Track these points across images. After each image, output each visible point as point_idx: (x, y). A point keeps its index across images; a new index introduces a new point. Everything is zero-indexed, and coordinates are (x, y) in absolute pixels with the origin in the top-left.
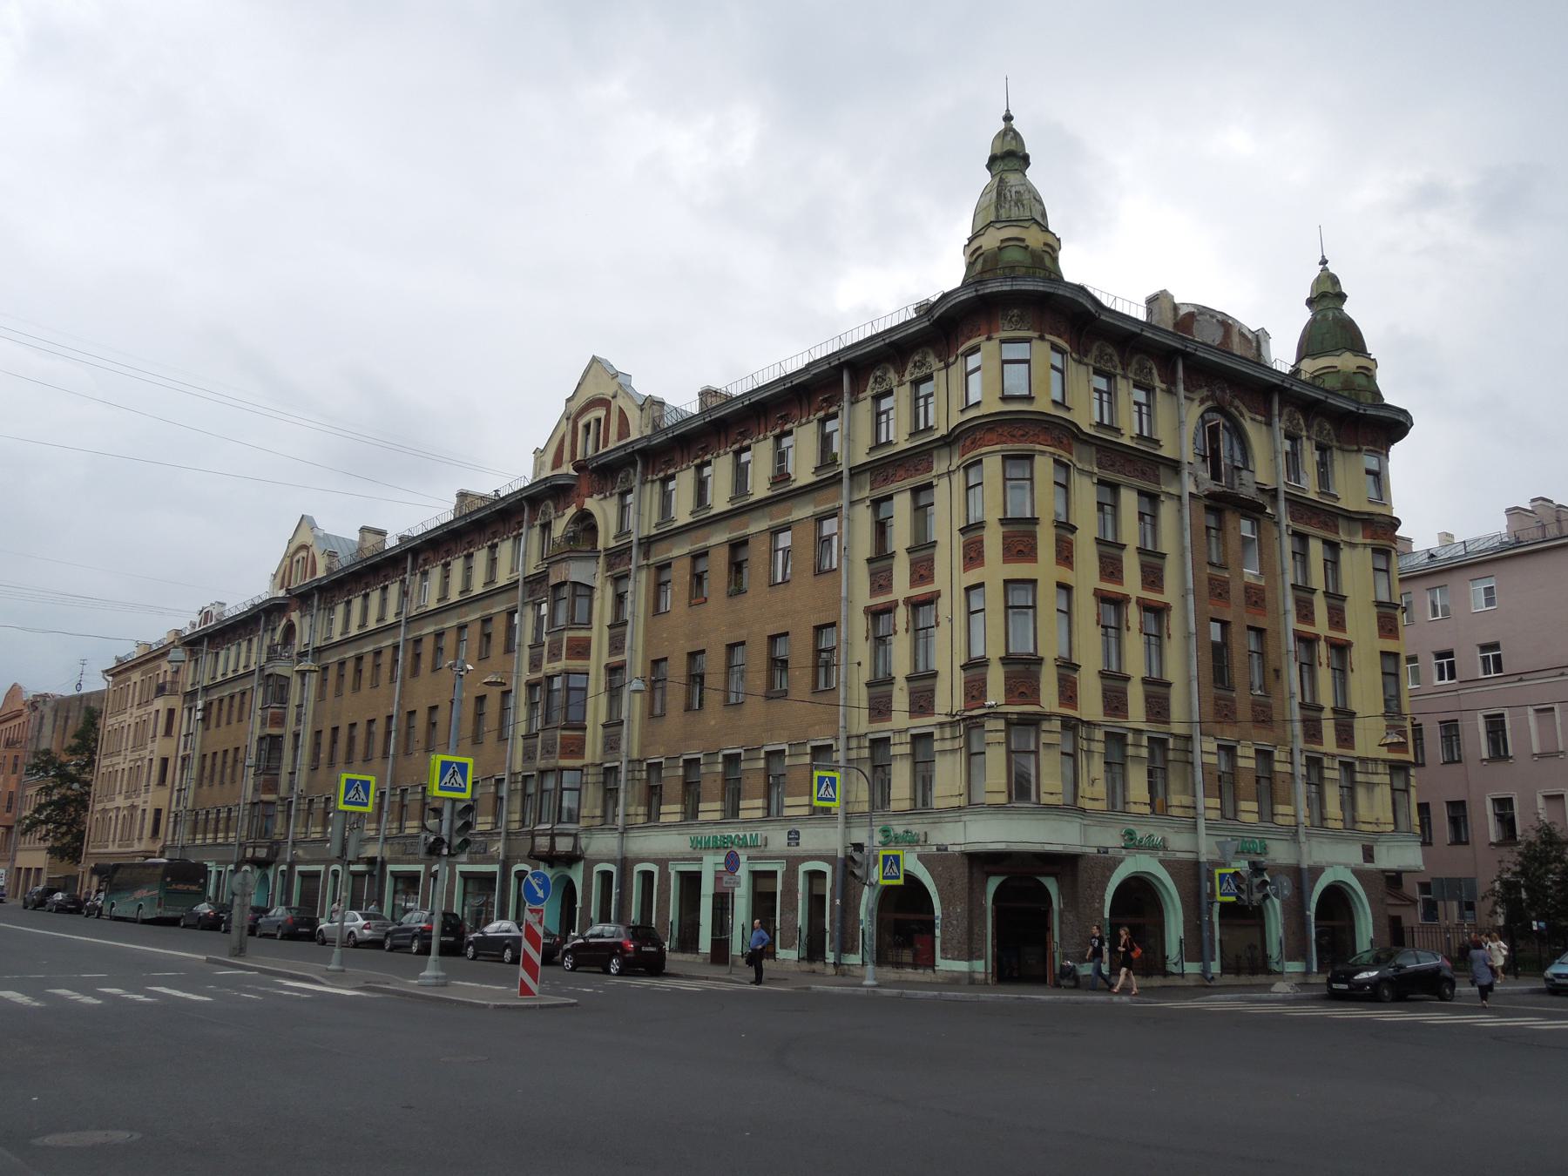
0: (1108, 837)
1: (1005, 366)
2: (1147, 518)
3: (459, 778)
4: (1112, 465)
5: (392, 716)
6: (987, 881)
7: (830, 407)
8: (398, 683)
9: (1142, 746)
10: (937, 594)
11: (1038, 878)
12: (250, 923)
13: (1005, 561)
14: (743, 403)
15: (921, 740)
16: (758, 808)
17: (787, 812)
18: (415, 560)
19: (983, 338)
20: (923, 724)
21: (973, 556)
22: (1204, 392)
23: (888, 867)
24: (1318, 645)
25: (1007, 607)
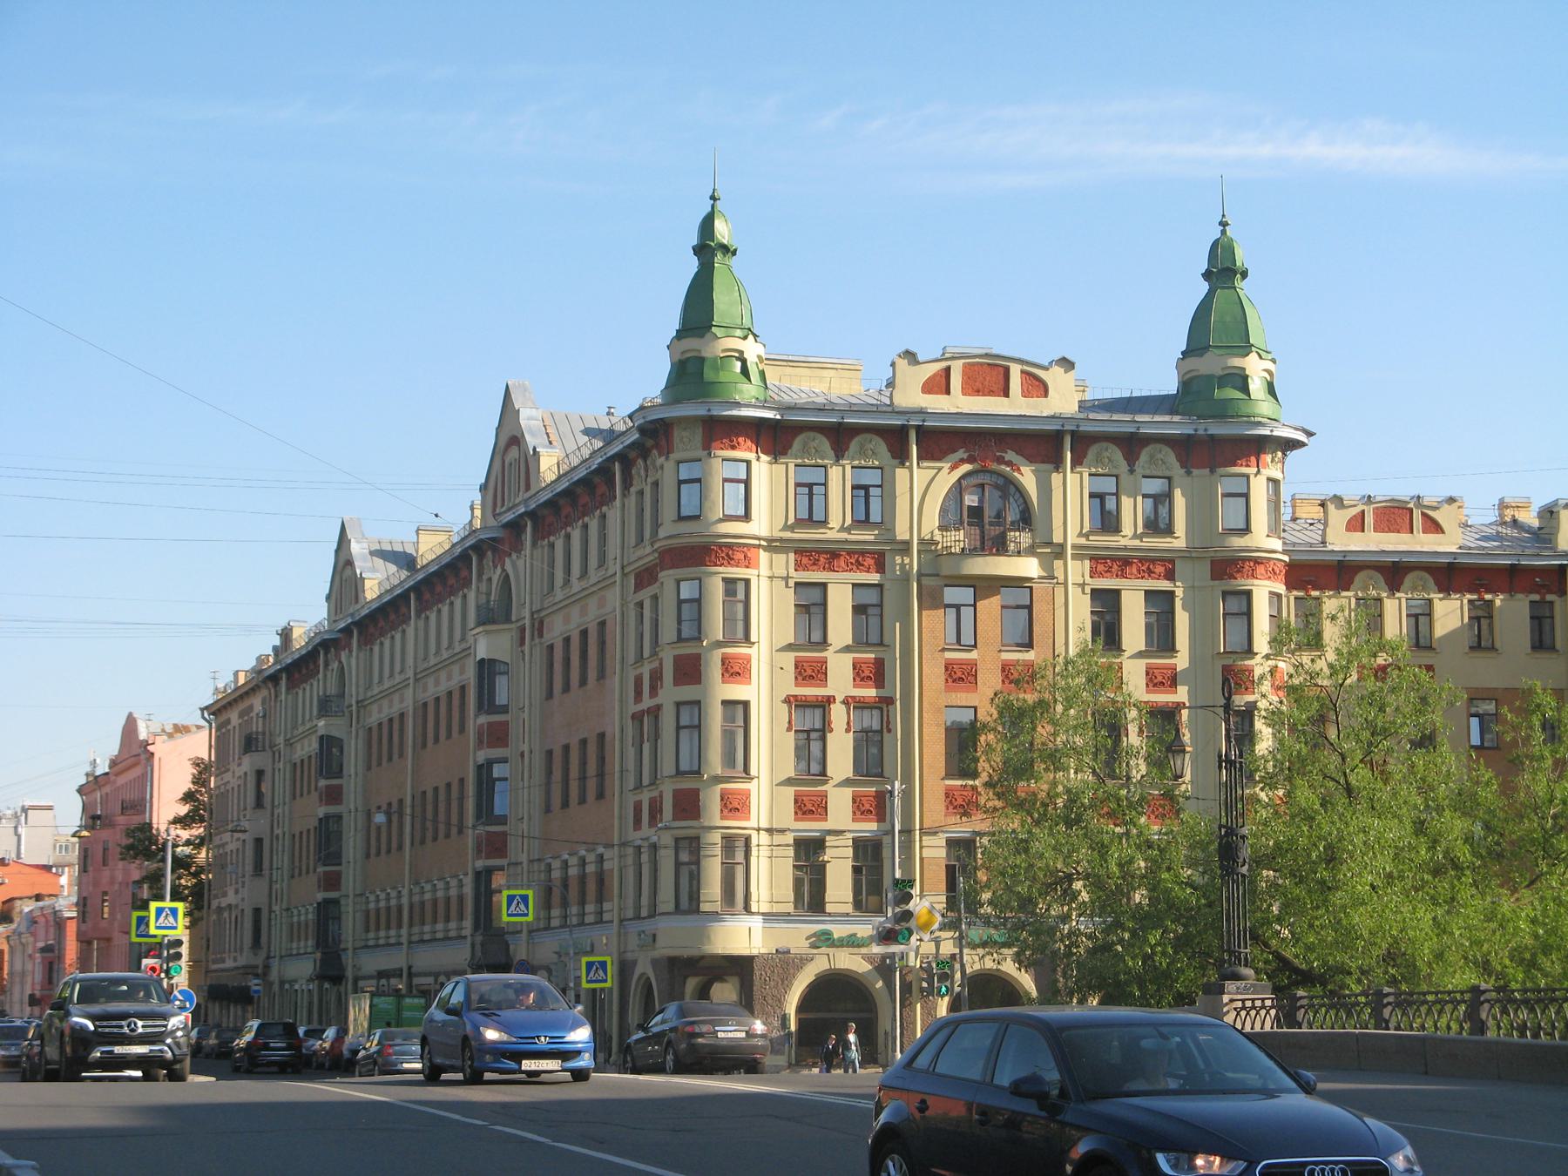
0: (796, 936)
3: (522, 906)
4: (814, 564)
6: (685, 983)
18: (419, 599)
22: (961, 454)
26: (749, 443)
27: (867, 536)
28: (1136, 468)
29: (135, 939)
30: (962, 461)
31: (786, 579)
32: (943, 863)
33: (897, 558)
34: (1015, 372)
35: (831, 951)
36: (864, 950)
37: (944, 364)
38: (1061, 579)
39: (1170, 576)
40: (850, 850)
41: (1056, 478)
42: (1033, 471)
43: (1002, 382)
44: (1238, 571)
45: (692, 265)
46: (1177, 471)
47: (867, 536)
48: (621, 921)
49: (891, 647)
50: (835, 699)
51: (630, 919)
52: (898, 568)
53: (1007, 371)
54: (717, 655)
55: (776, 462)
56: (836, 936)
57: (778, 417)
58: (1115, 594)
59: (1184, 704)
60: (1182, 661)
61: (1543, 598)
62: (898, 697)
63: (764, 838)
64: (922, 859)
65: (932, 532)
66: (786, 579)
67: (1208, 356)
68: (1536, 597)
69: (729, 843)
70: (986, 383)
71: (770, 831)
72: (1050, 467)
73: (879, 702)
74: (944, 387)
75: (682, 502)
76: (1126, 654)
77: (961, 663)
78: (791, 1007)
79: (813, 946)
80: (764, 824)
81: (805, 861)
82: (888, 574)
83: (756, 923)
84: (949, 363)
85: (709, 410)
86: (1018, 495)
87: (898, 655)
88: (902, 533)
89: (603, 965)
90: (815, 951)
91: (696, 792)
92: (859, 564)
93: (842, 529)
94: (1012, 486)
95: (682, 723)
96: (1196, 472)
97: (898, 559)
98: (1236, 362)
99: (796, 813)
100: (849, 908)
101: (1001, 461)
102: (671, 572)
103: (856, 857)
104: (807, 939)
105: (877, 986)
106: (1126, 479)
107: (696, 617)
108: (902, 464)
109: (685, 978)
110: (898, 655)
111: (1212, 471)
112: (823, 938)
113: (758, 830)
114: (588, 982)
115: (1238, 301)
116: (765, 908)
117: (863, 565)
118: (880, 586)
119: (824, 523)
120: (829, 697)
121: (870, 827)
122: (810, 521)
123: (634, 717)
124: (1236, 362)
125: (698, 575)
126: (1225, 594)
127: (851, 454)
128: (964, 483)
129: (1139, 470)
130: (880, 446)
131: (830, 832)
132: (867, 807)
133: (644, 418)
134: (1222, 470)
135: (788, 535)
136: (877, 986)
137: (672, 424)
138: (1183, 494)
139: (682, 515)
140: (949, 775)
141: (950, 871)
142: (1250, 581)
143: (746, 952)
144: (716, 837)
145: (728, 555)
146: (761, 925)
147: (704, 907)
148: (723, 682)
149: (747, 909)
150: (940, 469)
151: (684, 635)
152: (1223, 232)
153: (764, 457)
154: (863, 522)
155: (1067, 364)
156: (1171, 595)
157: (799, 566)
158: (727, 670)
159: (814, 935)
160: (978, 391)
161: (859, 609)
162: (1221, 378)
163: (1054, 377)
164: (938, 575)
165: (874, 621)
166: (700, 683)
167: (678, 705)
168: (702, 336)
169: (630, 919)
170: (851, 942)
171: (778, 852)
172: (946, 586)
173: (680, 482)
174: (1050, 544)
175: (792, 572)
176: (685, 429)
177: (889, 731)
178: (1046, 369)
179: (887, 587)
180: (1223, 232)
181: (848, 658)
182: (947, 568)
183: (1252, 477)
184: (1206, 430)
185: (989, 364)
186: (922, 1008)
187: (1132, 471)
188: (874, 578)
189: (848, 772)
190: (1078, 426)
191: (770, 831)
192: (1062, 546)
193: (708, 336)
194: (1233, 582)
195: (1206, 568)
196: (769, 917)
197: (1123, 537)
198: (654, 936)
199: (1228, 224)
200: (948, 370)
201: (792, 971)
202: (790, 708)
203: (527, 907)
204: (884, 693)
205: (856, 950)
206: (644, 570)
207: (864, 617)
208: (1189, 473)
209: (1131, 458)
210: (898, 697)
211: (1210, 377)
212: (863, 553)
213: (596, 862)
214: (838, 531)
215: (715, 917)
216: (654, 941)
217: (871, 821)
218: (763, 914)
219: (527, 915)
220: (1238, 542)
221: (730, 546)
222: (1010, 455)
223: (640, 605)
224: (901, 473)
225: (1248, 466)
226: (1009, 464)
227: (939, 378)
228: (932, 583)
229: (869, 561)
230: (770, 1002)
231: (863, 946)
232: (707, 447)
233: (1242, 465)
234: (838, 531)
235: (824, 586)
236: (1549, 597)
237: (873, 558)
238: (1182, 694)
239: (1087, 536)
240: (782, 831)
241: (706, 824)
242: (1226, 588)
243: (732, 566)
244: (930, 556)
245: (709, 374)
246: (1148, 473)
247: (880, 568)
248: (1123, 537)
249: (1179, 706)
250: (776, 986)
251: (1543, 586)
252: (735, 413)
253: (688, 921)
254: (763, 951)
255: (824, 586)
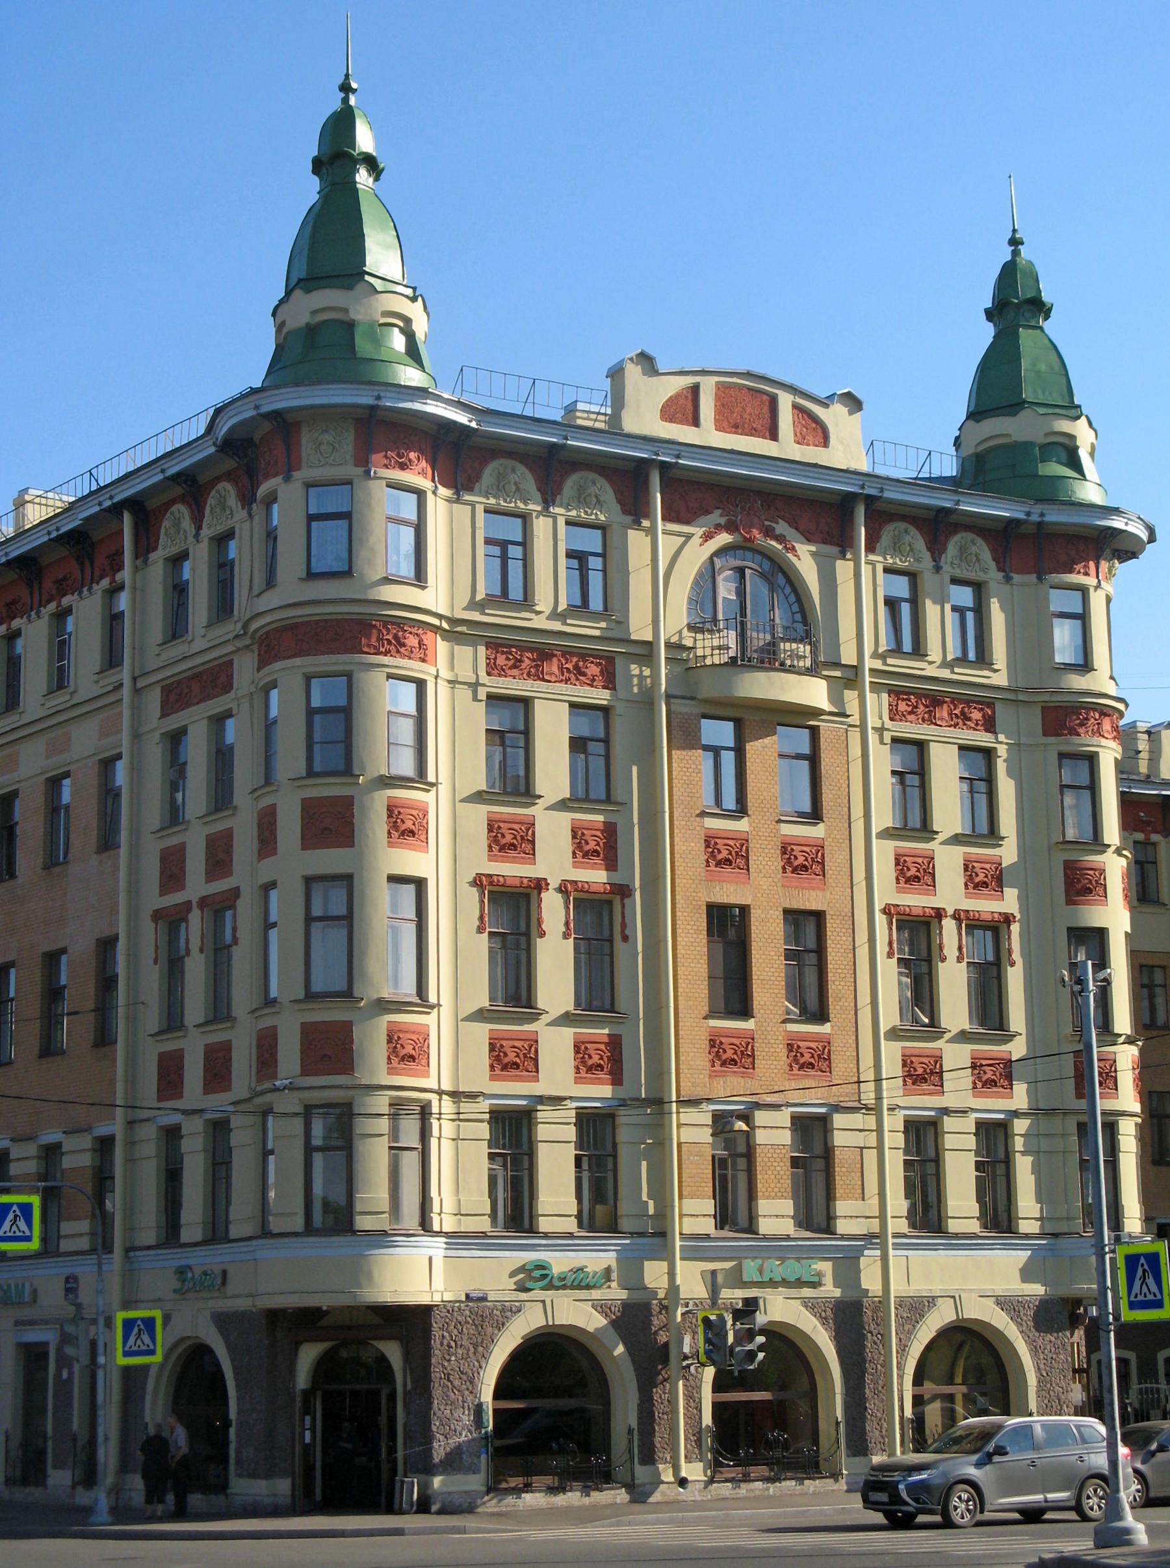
1: (314, 524)
2: (596, 748)
3: (22, 1224)
4: (514, 667)
5: (114, 939)
6: (296, 1354)
7: (13, 618)
8: (123, 851)
9: (1021, 1135)
10: (235, 893)
11: (334, 1343)
12: (1132, 1537)
13: (303, 849)
14: (100, 504)
15: (219, 1128)
16: (81, 1235)
17: (65, 1245)
19: (279, 479)
20: (220, 1101)
21: (267, 842)
22: (716, 517)
23: (1137, 1283)
24: (941, 928)
25: (309, 919)
26: (424, 464)
27: (592, 629)
28: (942, 563)
29: (120, 1316)
30: (719, 528)
31: (475, 686)
32: (709, 1152)
33: (633, 666)
34: (785, 401)
35: (548, 1295)
36: (596, 1294)
37: (689, 380)
38: (855, 719)
39: (990, 725)
40: (572, 1130)
41: (844, 569)
42: (813, 554)
43: (768, 416)
44: (1082, 725)
45: (310, 189)
46: (993, 575)
47: (592, 629)
48: (128, 1250)
49: (626, 805)
50: (548, 884)
51: (149, 1248)
52: (635, 681)
53: (773, 402)
54: (380, 799)
55: (458, 500)
56: (556, 1270)
57: (474, 425)
58: (921, 746)
59: (1014, 917)
60: (1008, 853)
61: (1148, 839)
62: (637, 884)
63: (447, 1105)
64: (679, 1145)
65: (680, 632)
66: (475, 686)
67: (1025, 415)
68: (1140, 836)
69: (398, 1108)
70: (746, 416)
71: (455, 1095)
72: (834, 550)
73: (612, 892)
74: (690, 416)
75: (314, 552)
76: (940, 838)
77: (727, 836)
78: (487, 1395)
79: (522, 1288)
80: (446, 1086)
81: (510, 1148)
82: (621, 693)
83: (436, 1247)
84: (697, 379)
85: (378, 398)
86: (788, 590)
87: (636, 820)
88: (640, 630)
89: (149, 1323)
90: (524, 1296)
91: (346, 1028)
92: (579, 672)
93: (554, 615)
94: (780, 575)
95: (317, 911)
96: (1016, 578)
97: (635, 669)
98: (1065, 426)
99: (492, 1067)
100: (571, 1225)
101: (769, 533)
102: (297, 661)
103: (580, 1144)
104: (512, 1275)
105: (616, 1353)
106: (929, 580)
107: (341, 736)
108: (637, 524)
109: (298, 1344)
110: (636, 820)
111: (1040, 578)
112: (537, 1273)
113: (440, 1093)
114: (126, 1354)
115: (1049, 345)
116: (449, 1225)
117: (584, 674)
118: (605, 710)
119: (527, 602)
120: (539, 880)
121: (600, 1092)
122: (501, 599)
123: (157, 916)
124: (1065, 426)
125: (347, 668)
126: (1062, 756)
127: (565, 500)
128: (718, 563)
129: (948, 570)
130: (604, 489)
131: (541, 1099)
132: (596, 1059)
133: (257, 407)
134: (1055, 578)
135: (476, 616)
136: (616, 1353)
137: (298, 424)
138: (1003, 609)
139: (314, 570)
140: (713, 1014)
141: (719, 1164)
142: (1096, 740)
143: (424, 1299)
144: (381, 1103)
145: (396, 637)
146: (442, 1252)
147: (363, 1223)
148: (391, 845)
149: (425, 1224)
150: (689, 537)
151: (317, 768)
152: (1015, 253)
153: (443, 491)
154: (581, 608)
155: (853, 402)
156: (988, 754)
157: (492, 669)
158: (395, 826)
159: (522, 1269)
160: (736, 426)
161: (578, 744)
162: (1043, 447)
163: (835, 417)
164: (693, 698)
165: (598, 764)
166: (353, 846)
167: (309, 881)
168: (350, 287)
169: (149, 1248)
170: (577, 1282)
171: (469, 1129)
172: (705, 716)
173: (311, 518)
174: (837, 665)
175: (484, 678)
176: (326, 431)
177: (625, 938)
178: (826, 406)
179: (620, 708)
180: (1015, 253)
181: (565, 820)
182: (708, 689)
183: (1092, 590)
184: (1042, 515)
185: (750, 389)
186: (684, 1385)
187: (938, 569)
188: (600, 696)
189: (566, 1002)
190: (882, 490)
191: (455, 1095)
192: (856, 669)
193: (360, 287)
194: (1075, 739)
195: (1035, 718)
196: (455, 1239)
197: (931, 663)
198: (224, 1273)
199: (1022, 243)
200: (695, 389)
201: (489, 1330)
202: (482, 895)
203: (29, 1224)
204: (619, 878)
205: (794, 1292)
206: (190, 679)
207: (582, 756)
208: (1008, 579)
209: (936, 548)
210: (637, 884)
211: (1027, 446)
212: (584, 655)
213: (94, 1150)
214: (548, 618)
215: (381, 1238)
216: (224, 1283)
217: (600, 1082)
218: (448, 1235)
219: (28, 1239)
220: (1078, 682)
221: (400, 623)
222: (781, 527)
223: (176, 738)
224: (637, 541)
225: (1086, 574)
226: (780, 539)
227: (682, 401)
228: (684, 710)
229: (593, 670)
230: (457, 1383)
231: (594, 1287)
232: (363, 461)
233: (1079, 572)
234: (548, 618)
235: (526, 703)
236: (1155, 837)
237: (597, 664)
238: (1009, 902)
239: (883, 657)
240: (472, 1096)
241: (364, 1082)
242: (1065, 749)
243: (403, 656)
244: (679, 669)
245: (363, 346)
246: (958, 573)
247: (609, 682)
248: (931, 663)
249: (1008, 919)
250: (465, 1357)
251: (1148, 823)
252: (417, 406)
253: (335, 1247)
254: (448, 1297)
255: (526, 703)
